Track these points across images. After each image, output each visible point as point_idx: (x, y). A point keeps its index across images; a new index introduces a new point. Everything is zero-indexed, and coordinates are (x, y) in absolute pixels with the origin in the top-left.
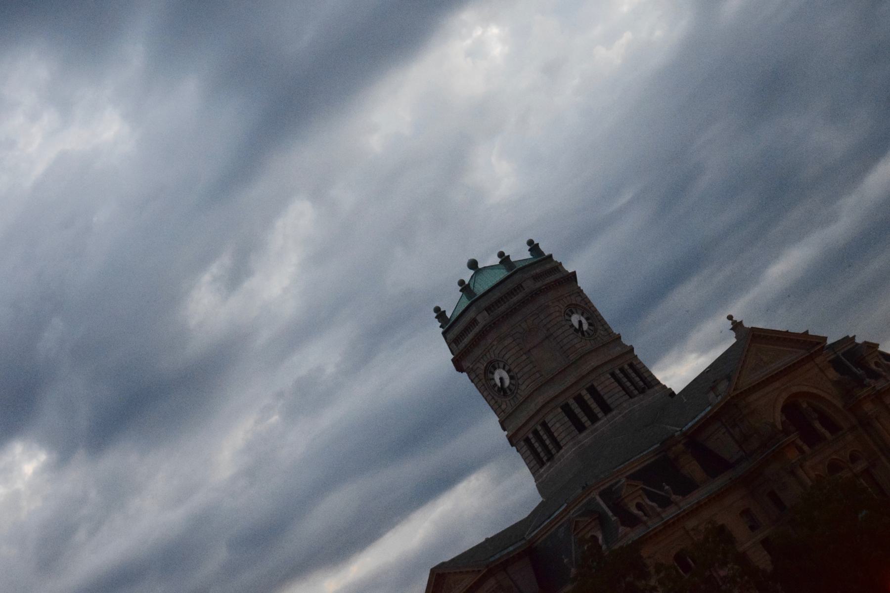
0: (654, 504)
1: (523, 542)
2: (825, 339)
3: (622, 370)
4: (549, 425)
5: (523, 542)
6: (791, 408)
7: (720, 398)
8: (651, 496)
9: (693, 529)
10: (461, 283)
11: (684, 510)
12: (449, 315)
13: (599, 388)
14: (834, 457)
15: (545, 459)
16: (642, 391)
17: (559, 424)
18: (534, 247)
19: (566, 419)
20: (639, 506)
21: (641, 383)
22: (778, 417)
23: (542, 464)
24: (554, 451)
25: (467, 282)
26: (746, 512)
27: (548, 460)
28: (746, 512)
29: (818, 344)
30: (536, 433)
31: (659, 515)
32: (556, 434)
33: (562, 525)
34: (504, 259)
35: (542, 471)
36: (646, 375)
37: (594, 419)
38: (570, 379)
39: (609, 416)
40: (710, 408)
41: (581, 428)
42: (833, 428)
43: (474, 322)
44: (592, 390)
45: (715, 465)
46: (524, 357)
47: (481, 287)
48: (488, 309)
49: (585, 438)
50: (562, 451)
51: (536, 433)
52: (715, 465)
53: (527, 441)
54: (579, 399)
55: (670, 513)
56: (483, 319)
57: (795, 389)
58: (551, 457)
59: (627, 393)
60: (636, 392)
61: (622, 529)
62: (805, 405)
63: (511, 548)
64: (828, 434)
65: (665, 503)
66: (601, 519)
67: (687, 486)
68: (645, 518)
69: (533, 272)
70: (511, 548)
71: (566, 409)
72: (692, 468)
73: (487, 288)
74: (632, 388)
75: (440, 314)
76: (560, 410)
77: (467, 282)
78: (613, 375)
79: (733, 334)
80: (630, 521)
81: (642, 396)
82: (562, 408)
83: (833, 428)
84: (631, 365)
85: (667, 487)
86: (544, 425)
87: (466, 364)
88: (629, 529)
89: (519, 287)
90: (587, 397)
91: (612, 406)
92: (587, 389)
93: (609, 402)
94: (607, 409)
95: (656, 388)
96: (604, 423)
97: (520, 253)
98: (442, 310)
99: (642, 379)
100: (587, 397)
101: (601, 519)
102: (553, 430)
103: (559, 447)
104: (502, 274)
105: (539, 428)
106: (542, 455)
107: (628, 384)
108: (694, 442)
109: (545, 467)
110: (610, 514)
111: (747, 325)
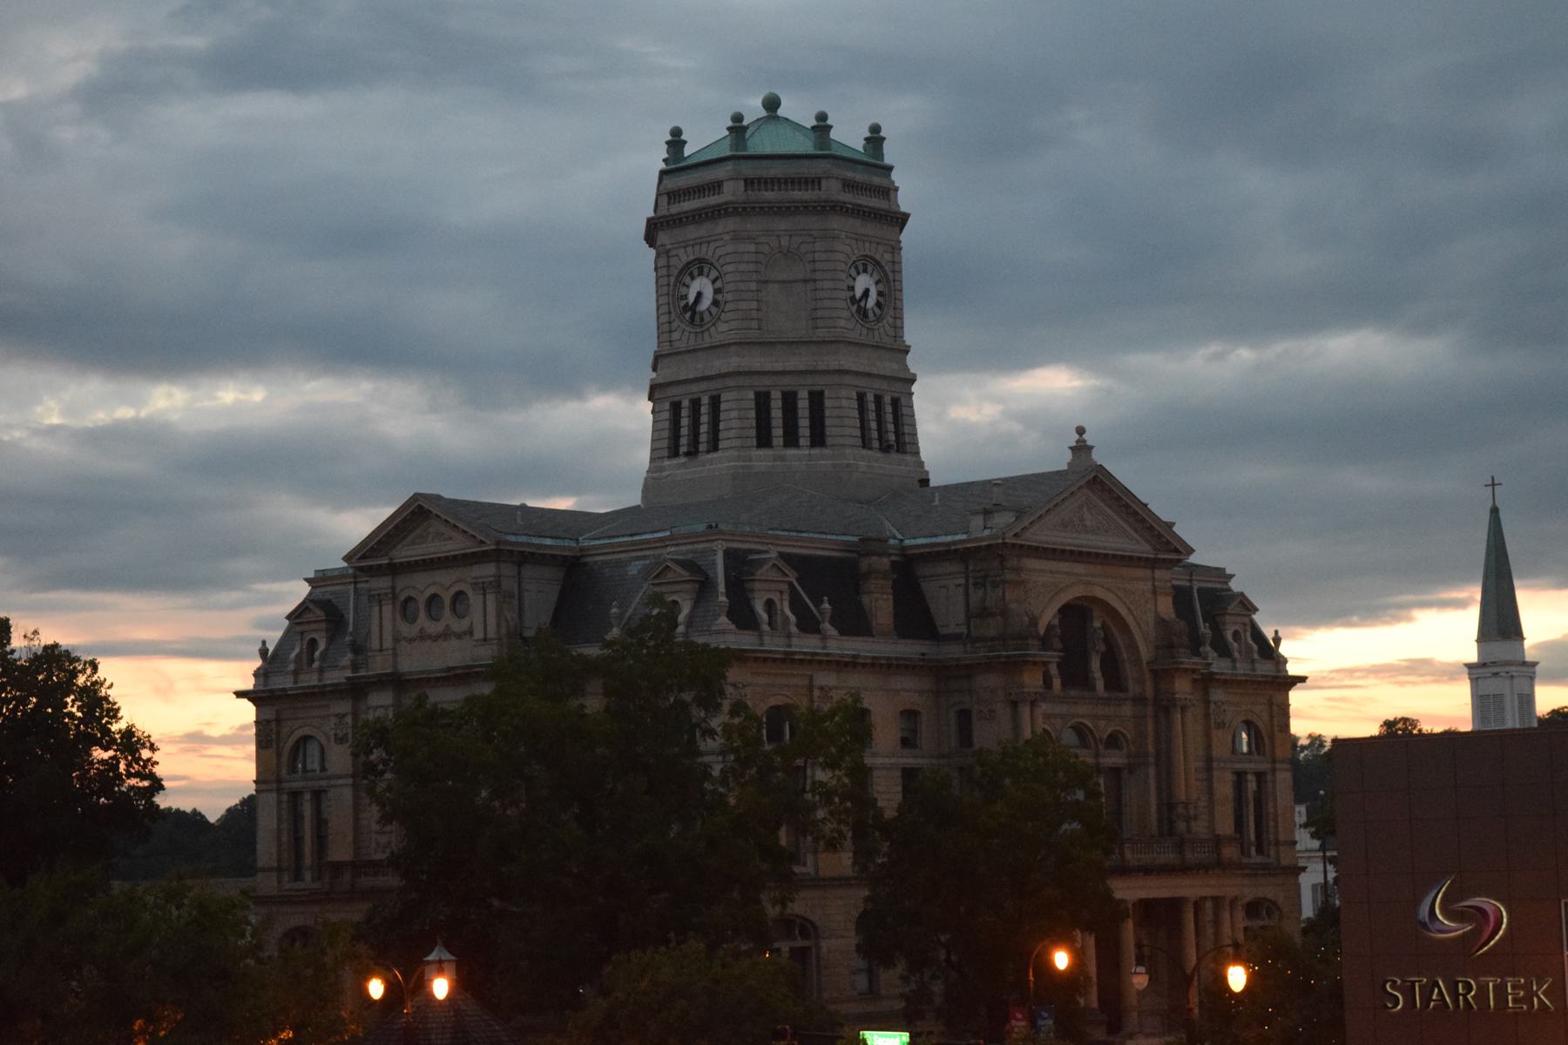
0: (792, 618)
1: (573, 544)
2: (1191, 551)
3: (878, 399)
4: (723, 406)
5: (573, 544)
6: (1076, 614)
7: (987, 532)
8: (796, 603)
9: (821, 688)
10: (738, 118)
11: (828, 655)
12: (687, 151)
13: (828, 403)
14: (1086, 722)
15: (683, 449)
16: (885, 448)
17: (737, 414)
18: (875, 139)
19: (753, 414)
20: (770, 605)
21: (892, 437)
22: (1048, 616)
23: (674, 453)
24: (702, 447)
25: (745, 123)
26: (910, 715)
27: (687, 454)
28: (910, 715)
29: (1177, 551)
30: (696, 404)
31: (789, 636)
32: (722, 426)
33: (638, 558)
34: (822, 126)
35: (667, 463)
36: (906, 429)
37: (791, 440)
38: (795, 362)
39: (816, 451)
40: (964, 537)
41: (764, 440)
42: (1115, 681)
43: (716, 186)
44: (817, 399)
45: (915, 618)
46: (753, 286)
47: (762, 143)
48: (749, 183)
49: (762, 459)
50: (715, 455)
51: (696, 404)
52: (915, 618)
53: (676, 407)
54: (789, 400)
55: (807, 644)
56: (732, 192)
57: (1099, 593)
58: (693, 453)
59: (863, 436)
60: (876, 444)
61: (723, 619)
62: (1097, 624)
63: (548, 542)
64: (1100, 685)
65: (808, 624)
66: (704, 586)
67: (854, 622)
68: (766, 627)
69: (849, 175)
70: (548, 542)
71: (762, 401)
72: (880, 604)
73: (768, 150)
74: (875, 434)
75: (676, 142)
76: (751, 395)
77: (745, 123)
78: (861, 398)
79: (1068, 456)
80: (743, 617)
81: (879, 455)
82: (758, 395)
83: (1115, 681)
84: (895, 403)
85: (826, 606)
86: (715, 402)
87: (663, 238)
88: (733, 627)
89: (815, 182)
90: (803, 404)
91: (829, 441)
92: (811, 393)
93: (828, 431)
94: (818, 439)
95: (908, 458)
96: (800, 457)
97: (849, 134)
98: (683, 137)
99: (897, 433)
100: (803, 404)
101: (704, 586)
102: (722, 416)
103: (714, 447)
104: (805, 146)
105: (686, 403)
106: (684, 441)
107: (874, 425)
108: (908, 572)
109: (675, 461)
110: (722, 588)
111: (1098, 457)
